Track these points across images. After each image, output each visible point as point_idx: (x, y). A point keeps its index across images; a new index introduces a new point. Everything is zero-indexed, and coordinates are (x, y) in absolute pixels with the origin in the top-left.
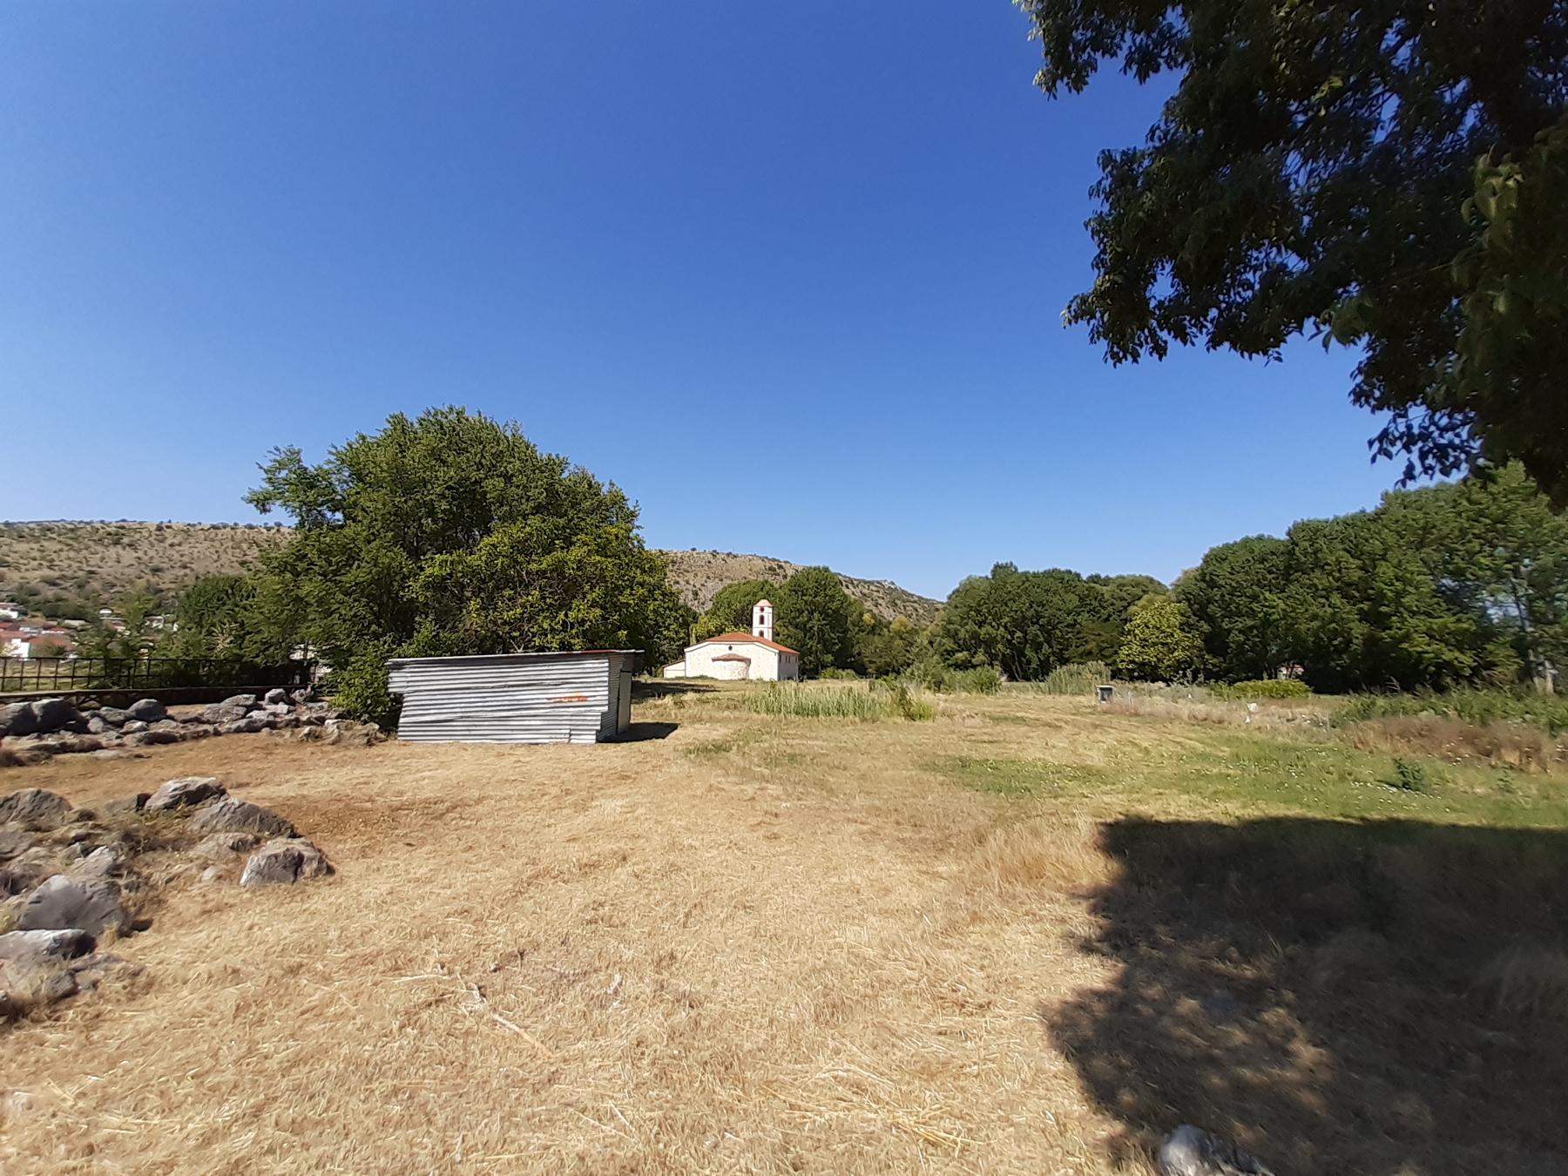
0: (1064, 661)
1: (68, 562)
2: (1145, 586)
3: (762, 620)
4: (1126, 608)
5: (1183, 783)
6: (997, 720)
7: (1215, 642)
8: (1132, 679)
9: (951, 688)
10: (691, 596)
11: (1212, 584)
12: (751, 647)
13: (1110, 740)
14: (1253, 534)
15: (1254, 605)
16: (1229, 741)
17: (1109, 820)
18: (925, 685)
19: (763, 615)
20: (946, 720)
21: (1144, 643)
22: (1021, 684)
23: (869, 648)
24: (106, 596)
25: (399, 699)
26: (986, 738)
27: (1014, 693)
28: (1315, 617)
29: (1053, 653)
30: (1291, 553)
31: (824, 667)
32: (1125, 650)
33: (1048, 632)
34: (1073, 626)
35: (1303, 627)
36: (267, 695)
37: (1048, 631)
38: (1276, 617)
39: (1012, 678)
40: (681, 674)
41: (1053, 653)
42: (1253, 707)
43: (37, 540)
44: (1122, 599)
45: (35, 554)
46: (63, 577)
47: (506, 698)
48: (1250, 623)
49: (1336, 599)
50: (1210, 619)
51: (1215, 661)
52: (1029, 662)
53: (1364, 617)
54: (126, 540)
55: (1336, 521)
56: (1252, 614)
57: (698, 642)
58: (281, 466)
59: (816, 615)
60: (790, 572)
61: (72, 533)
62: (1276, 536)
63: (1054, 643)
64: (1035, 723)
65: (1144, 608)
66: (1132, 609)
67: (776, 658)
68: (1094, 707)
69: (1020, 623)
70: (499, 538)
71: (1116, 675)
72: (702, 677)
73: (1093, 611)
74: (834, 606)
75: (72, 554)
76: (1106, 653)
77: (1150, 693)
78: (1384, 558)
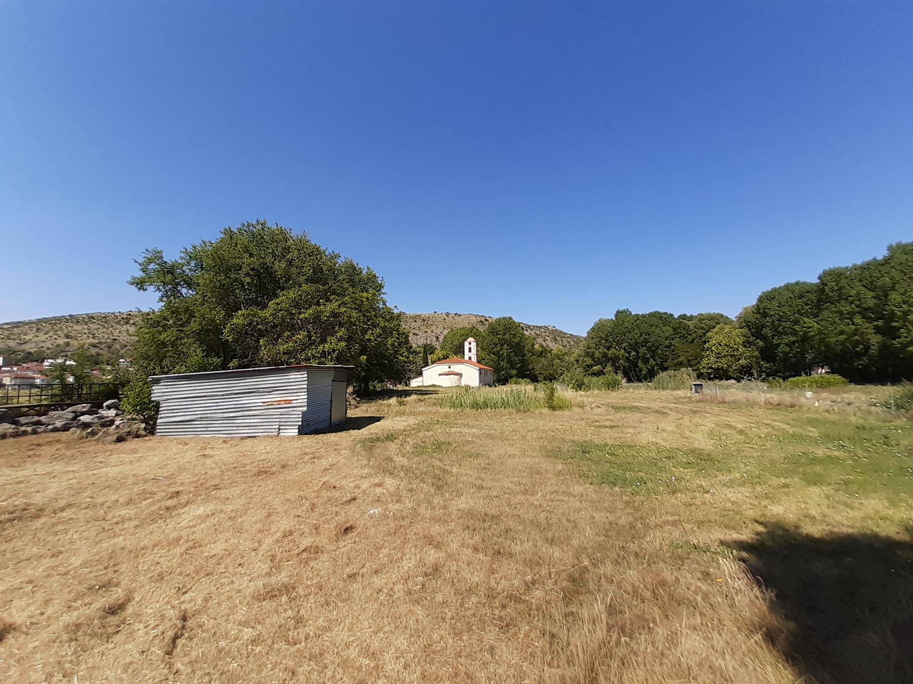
0: (664, 369)
1: (102, 335)
2: (716, 320)
3: (470, 350)
4: (705, 334)
5: (808, 470)
6: (617, 409)
7: (768, 353)
8: (710, 379)
9: (589, 388)
10: (434, 339)
11: (765, 315)
12: (462, 366)
13: (709, 423)
14: (793, 281)
15: (796, 327)
16: (813, 422)
17: (746, 535)
18: (571, 386)
19: (471, 347)
20: (577, 410)
21: (718, 356)
22: (636, 384)
23: (539, 365)
24: (122, 352)
25: (157, 406)
26: (608, 423)
27: (631, 390)
28: (842, 333)
29: (657, 364)
30: (822, 291)
31: (511, 377)
32: (705, 361)
33: (653, 351)
34: (669, 347)
35: (833, 340)
36: (105, 404)
37: (653, 351)
38: (812, 333)
39: (630, 380)
40: (421, 384)
41: (657, 364)
42: (809, 394)
43: (86, 323)
44: (702, 328)
45: (86, 331)
46: (100, 343)
47: (231, 403)
48: (793, 339)
49: (858, 319)
50: (764, 338)
51: (768, 365)
52: (641, 371)
53: (878, 330)
54: (131, 322)
55: (855, 268)
56: (795, 333)
57: (433, 363)
58: (150, 261)
59: (505, 346)
60: (490, 320)
61: (104, 319)
62: (814, 282)
63: (657, 358)
64: (647, 411)
65: (717, 333)
66: (709, 334)
67: (478, 373)
68: (690, 398)
69: (635, 347)
70: (285, 298)
71: (700, 376)
72: (433, 386)
73: (683, 337)
75: (104, 330)
76: (692, 363)
77: (728, 387)
78: (893, 288)
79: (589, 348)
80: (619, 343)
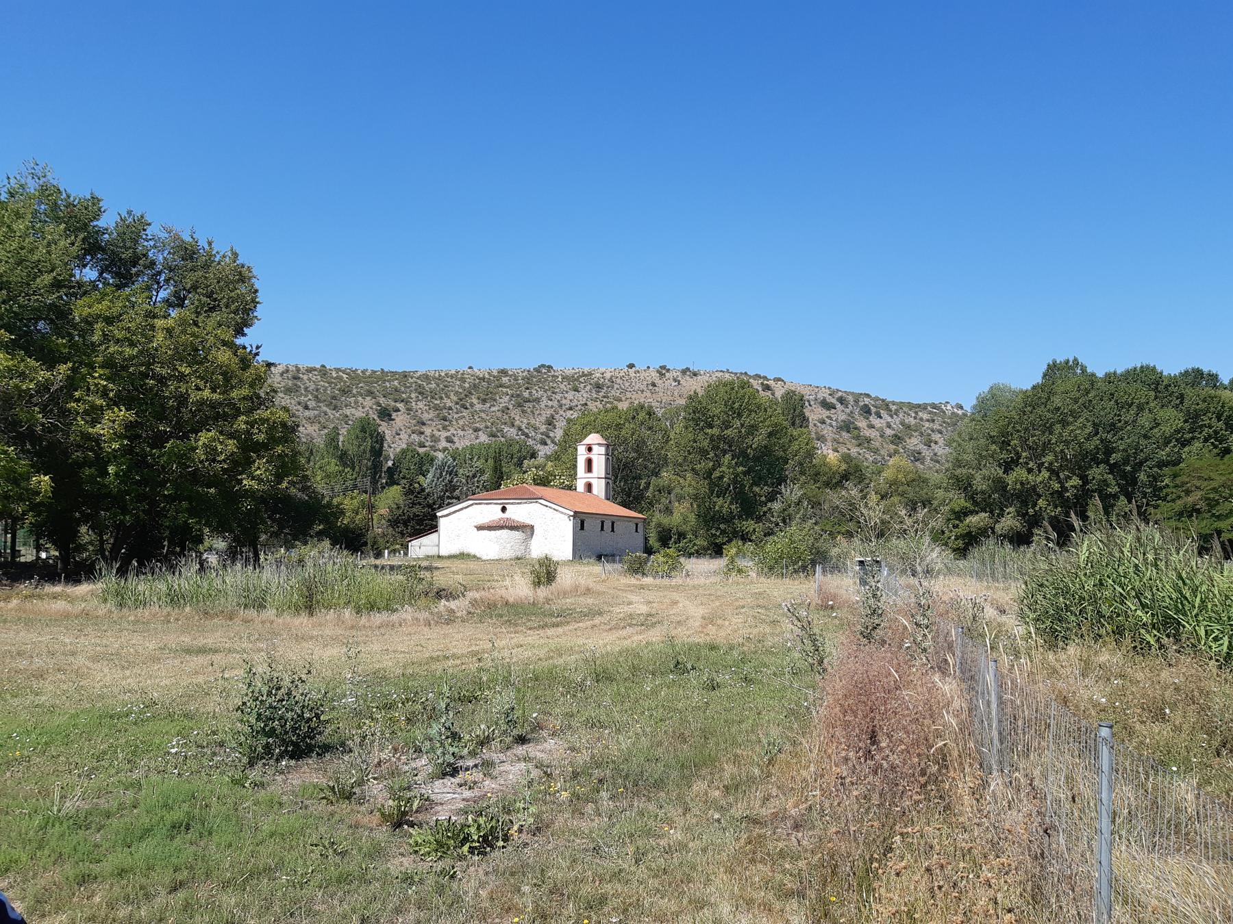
3: (589, 467)
74: (759, 439)
79: (958, 463)
80: (1038, 452)
